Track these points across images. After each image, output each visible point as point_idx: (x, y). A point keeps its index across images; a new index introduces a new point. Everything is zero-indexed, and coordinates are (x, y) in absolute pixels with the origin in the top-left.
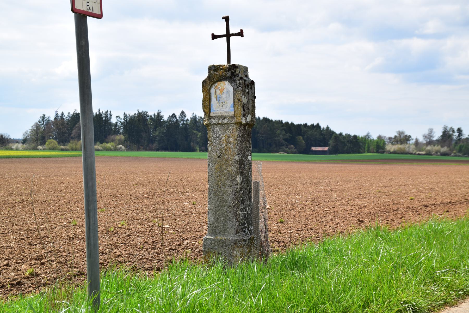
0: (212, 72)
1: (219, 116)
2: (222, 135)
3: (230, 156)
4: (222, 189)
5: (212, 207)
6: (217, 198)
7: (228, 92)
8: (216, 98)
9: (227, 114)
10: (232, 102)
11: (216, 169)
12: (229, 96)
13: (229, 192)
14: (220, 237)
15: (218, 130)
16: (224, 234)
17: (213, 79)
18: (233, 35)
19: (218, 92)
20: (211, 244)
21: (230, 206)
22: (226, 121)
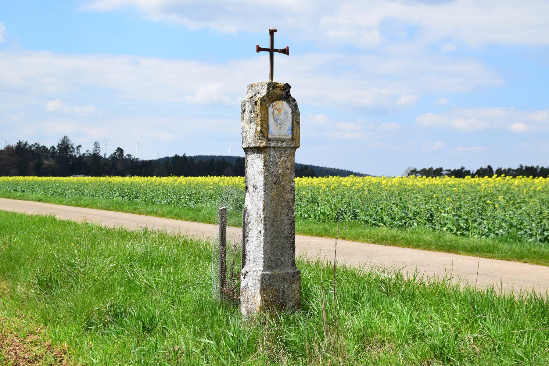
0: (271, 89)
1: (276, 138)
2: (278, 160)
3: (287, 182)
4: (279, 219)
5: (268, 239)
6: (273, 228)
7: (286, 113)
8: (274, 118)
9: (285, 137)
10: (290, 125)
11: (272, 197)
12: (287, 117)
13: (286, 221)
14: (277, 272)
15: (275, 154)
16: (280, 269)
17: (272, 97)
18: (277, 51)
19: (276, 112)
20: (269, 280)
21: (287, 237)
22: (284, 145)
